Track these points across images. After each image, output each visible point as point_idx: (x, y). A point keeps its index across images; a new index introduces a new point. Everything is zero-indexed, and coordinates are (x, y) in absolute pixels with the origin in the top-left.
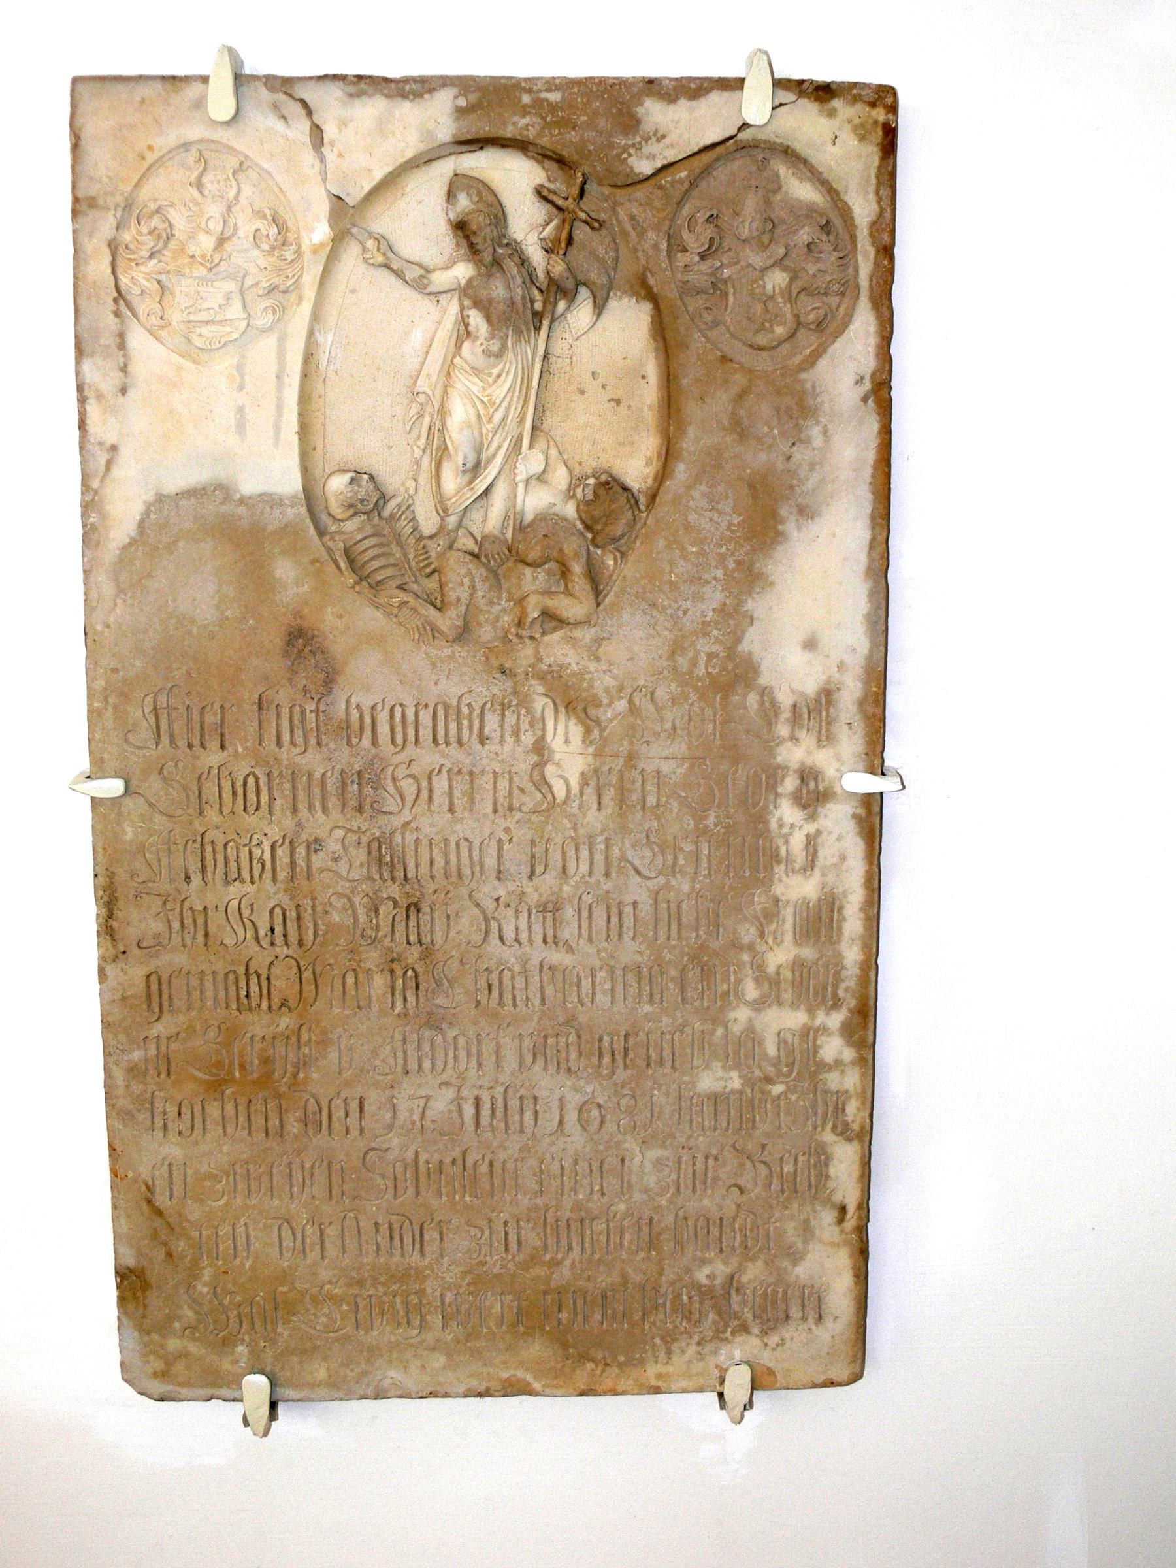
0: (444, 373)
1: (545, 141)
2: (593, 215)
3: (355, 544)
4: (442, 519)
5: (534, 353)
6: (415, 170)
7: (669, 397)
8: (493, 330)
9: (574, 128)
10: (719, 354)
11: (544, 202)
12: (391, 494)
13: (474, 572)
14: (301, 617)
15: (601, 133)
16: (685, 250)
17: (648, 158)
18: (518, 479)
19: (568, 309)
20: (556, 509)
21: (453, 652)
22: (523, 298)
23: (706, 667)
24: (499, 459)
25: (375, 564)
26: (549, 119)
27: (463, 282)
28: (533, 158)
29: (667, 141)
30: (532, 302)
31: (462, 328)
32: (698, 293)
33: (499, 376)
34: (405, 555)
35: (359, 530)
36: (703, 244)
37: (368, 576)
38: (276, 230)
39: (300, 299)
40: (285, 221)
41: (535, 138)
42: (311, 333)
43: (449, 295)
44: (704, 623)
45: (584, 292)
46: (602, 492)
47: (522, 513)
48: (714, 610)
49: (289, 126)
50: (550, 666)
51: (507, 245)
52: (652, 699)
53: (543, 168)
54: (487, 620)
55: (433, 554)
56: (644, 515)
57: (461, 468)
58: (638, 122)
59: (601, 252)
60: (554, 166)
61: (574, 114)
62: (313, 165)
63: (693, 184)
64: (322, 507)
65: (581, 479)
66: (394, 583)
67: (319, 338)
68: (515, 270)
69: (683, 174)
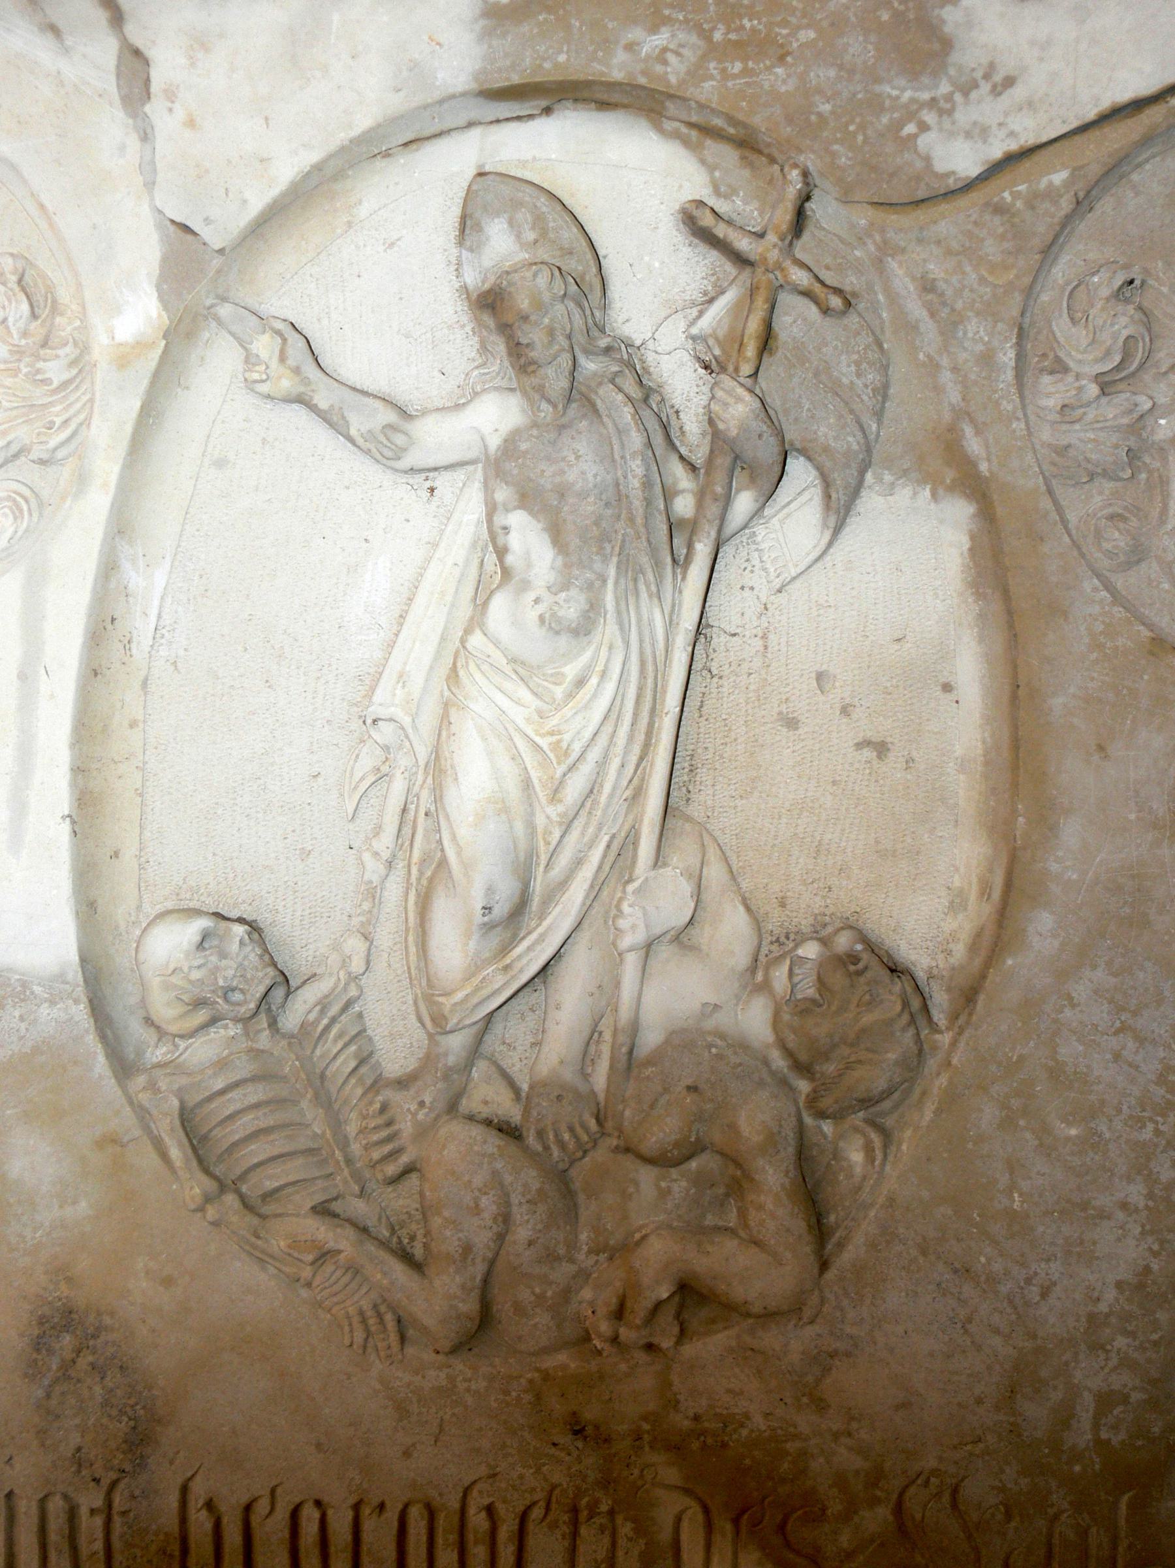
0: (443, 670)
1: (708, 91)
2: (829, 277)
3: (210, 1099)
4: (431, 1036)
5: (671, 624)
6: (379, 163)
7: (1016, 744)
8: (567, 566)
9: (781, 59)
10: (1146, 633)
11: (702, 248)
12: (306, 971)
13: (508, 1179)
14: (69, 1280)
15: (852, 72)
16: (1060, 368)
17: (968, 135)
18: (626, 942)
19: (758, 512)
20: (722, 1020)
21: (451, 1379)
22: (647, 484)
23: (1096, 1426)
24: (577, 893)
25: (258, 1151)
26: (718, 36)
27: (494, 442)
28: (675, 135)
29: (1018, 92)
30: (669, 495)
31: (491, 558)
32: (1092, 476)
33: (580, 682)
34: (336, 1124)
35: (222, 1065)
36: (1108, 353)
37: (243, 1177)
38: (25, 307)
39: (82, 480)
40: (50, 290)
41: (682, 82)
42: (109, 568)
43: (460, 475)
44: (1092, 1317)
45: (799, 471)
46: (838, 980)
47: (635, 1027)
48: (1119, 1285)
49: (67, 51)
50: (697, 1418)
51: (608, 350)
52: (954, 1505)
53: (703, 162)
54: (541, 1297)
55: (406, 1127)
56: (945, 1039)
57: (479, 918)
58: (947, 44)
59: (845, 370)
60: (728, 155)
61: (784, 23)
62: (122, 148)
63: (1083, 204)
64: (133, 1000)
65: (788, 940)
66: (306, 1200)
67: (134, 578)
68: (627, 412)
69: (1059, 178)
